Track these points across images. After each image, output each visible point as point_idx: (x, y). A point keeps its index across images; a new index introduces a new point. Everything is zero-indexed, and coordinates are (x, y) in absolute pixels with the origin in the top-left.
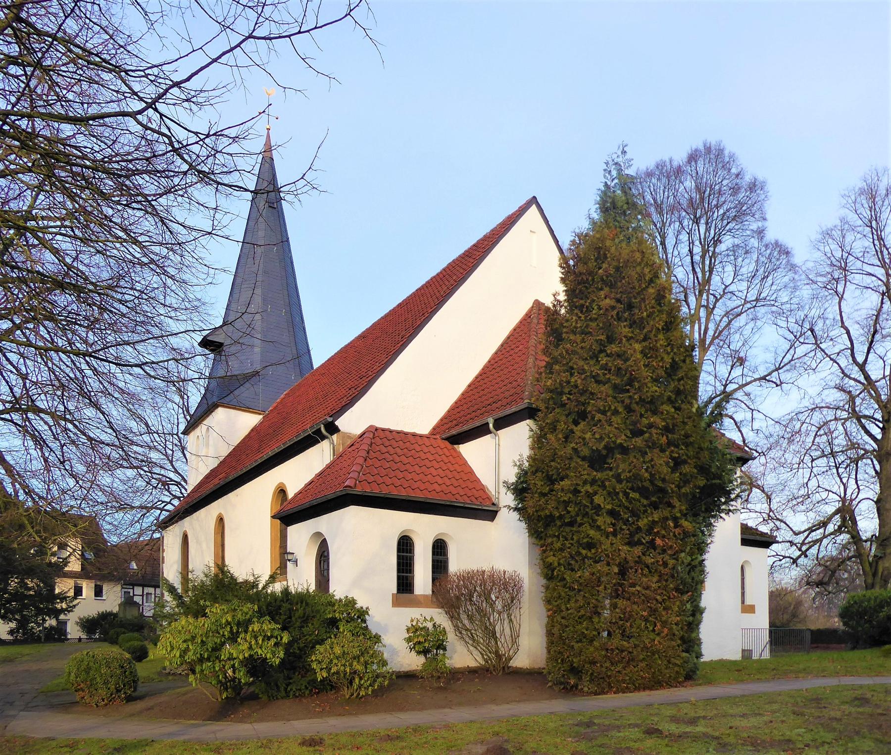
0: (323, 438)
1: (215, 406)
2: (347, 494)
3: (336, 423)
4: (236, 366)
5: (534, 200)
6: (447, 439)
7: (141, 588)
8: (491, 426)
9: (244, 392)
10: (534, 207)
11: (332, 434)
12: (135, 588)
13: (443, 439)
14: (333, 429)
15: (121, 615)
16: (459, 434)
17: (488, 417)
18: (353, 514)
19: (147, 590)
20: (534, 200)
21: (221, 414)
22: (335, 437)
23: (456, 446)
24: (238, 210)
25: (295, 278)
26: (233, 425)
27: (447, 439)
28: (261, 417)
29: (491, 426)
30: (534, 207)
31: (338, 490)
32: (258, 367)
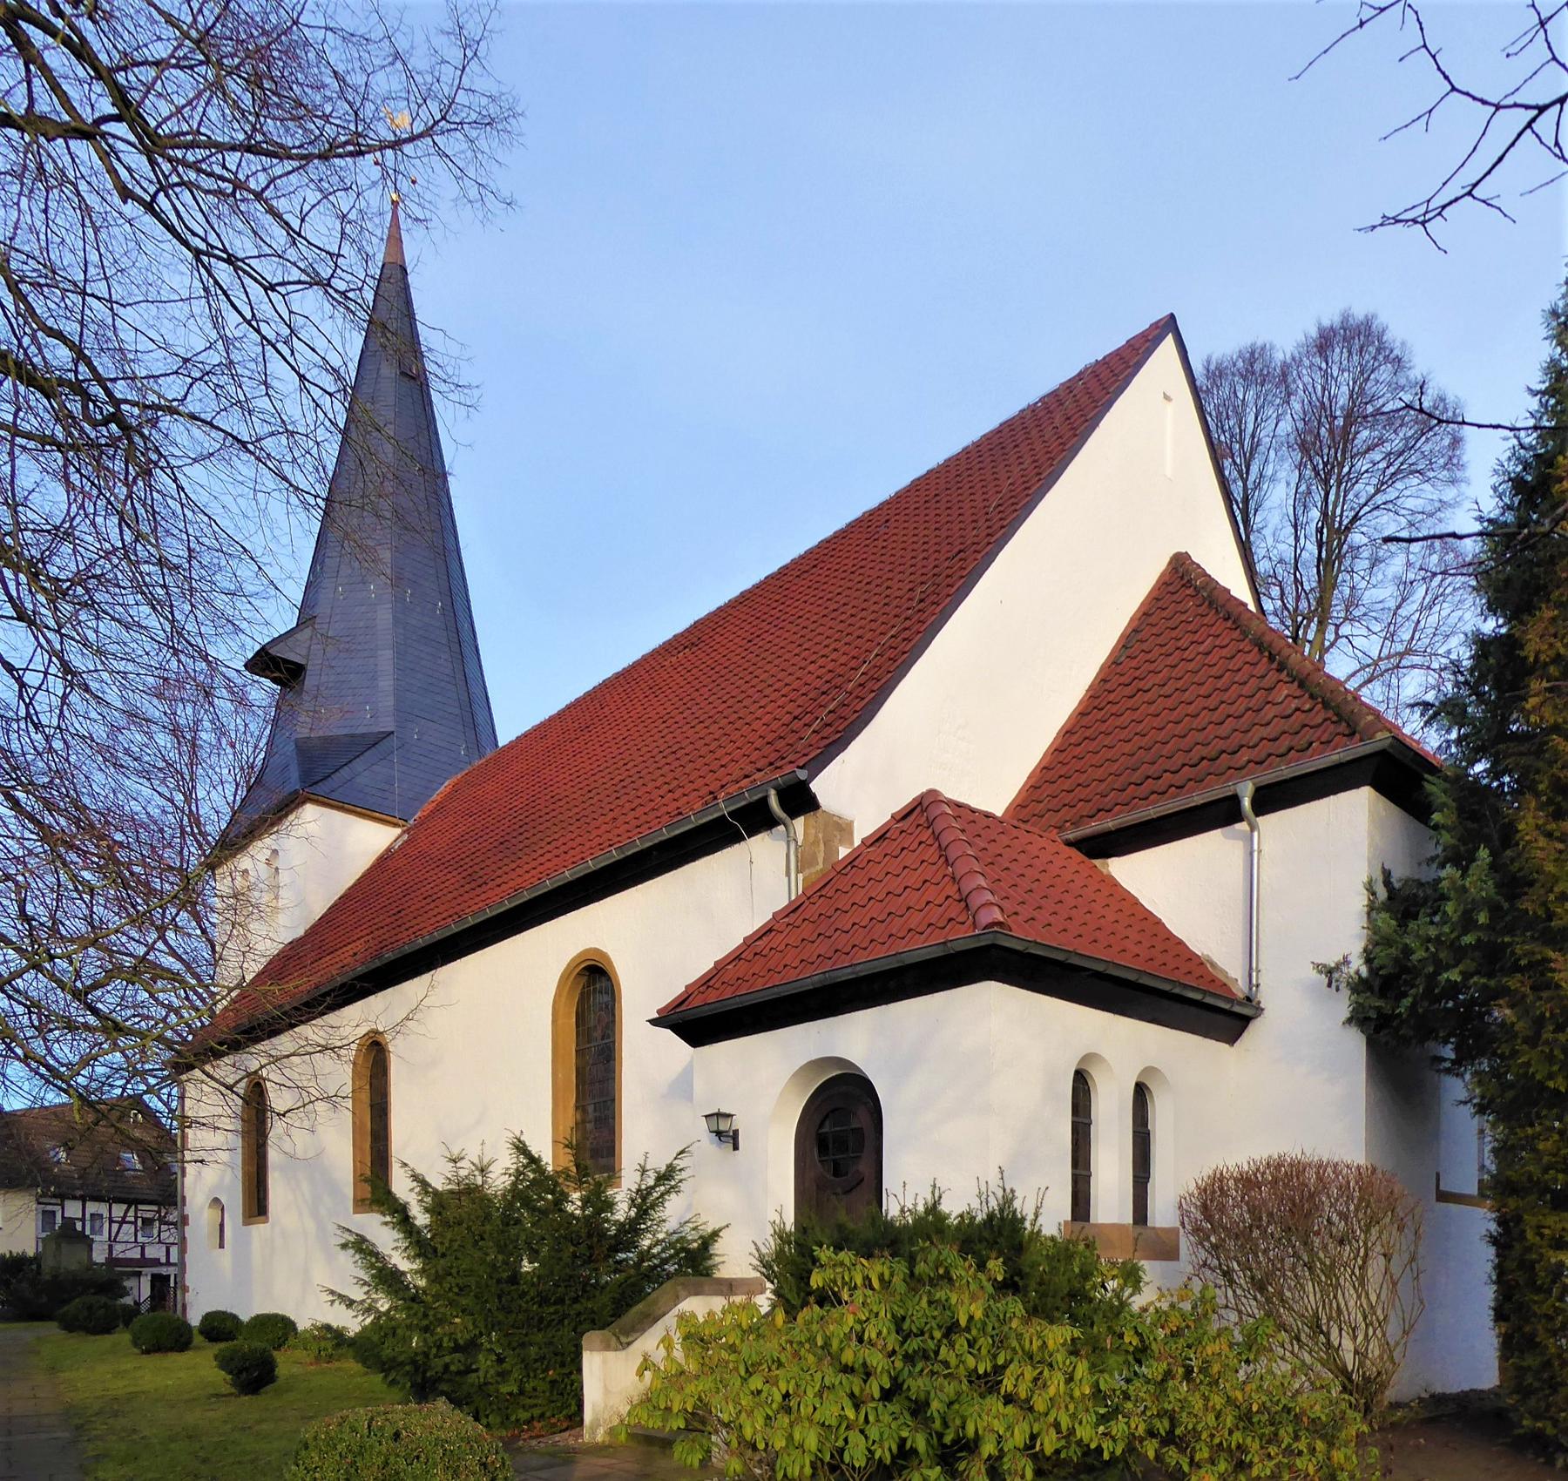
0: (769, 823)
1: (287, 806)
2: (994, 946)
3: (814, 786)
4: (323, 718)
5: (1170, 325)
6: (1076, 844)
7: (79, 1204)
8: (1246, 803)
9: (364, 773)
10: (1169, 340)
11: (793, 814)
12: (68, 1203)
13: (1069, 843)
14: (800, 800)
15: (48, 1264)
16: (1120, 831)
17: (1243, 779)
18: (992, 1012)
19: (92, 1207)
20: (1170, 325)
21: (311, 817)
22: (799, 823)
23: (1097, 862)
24: (341, 340)
25: (456, 538)
26: (327, 854)
27: (1076, 844)
28: (398, 831)
29: (1246, 803)
30: (1169, 340)
31: (961, 937)
32: (387, 724)
